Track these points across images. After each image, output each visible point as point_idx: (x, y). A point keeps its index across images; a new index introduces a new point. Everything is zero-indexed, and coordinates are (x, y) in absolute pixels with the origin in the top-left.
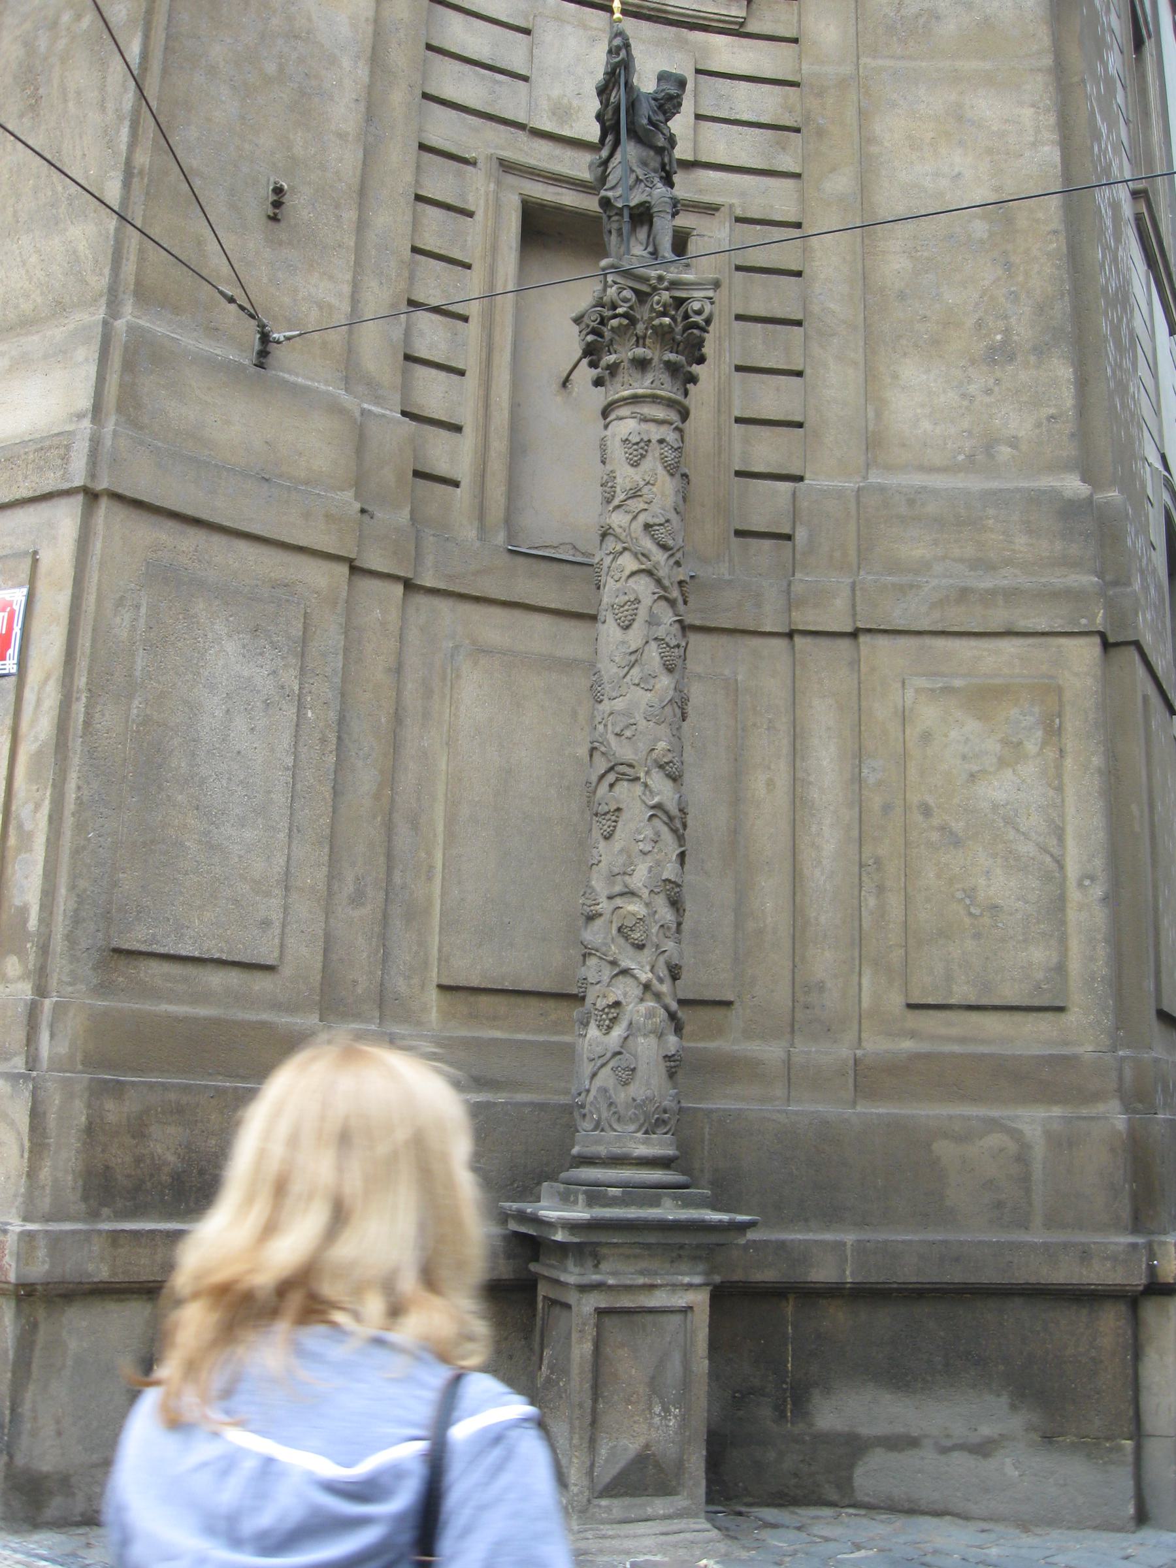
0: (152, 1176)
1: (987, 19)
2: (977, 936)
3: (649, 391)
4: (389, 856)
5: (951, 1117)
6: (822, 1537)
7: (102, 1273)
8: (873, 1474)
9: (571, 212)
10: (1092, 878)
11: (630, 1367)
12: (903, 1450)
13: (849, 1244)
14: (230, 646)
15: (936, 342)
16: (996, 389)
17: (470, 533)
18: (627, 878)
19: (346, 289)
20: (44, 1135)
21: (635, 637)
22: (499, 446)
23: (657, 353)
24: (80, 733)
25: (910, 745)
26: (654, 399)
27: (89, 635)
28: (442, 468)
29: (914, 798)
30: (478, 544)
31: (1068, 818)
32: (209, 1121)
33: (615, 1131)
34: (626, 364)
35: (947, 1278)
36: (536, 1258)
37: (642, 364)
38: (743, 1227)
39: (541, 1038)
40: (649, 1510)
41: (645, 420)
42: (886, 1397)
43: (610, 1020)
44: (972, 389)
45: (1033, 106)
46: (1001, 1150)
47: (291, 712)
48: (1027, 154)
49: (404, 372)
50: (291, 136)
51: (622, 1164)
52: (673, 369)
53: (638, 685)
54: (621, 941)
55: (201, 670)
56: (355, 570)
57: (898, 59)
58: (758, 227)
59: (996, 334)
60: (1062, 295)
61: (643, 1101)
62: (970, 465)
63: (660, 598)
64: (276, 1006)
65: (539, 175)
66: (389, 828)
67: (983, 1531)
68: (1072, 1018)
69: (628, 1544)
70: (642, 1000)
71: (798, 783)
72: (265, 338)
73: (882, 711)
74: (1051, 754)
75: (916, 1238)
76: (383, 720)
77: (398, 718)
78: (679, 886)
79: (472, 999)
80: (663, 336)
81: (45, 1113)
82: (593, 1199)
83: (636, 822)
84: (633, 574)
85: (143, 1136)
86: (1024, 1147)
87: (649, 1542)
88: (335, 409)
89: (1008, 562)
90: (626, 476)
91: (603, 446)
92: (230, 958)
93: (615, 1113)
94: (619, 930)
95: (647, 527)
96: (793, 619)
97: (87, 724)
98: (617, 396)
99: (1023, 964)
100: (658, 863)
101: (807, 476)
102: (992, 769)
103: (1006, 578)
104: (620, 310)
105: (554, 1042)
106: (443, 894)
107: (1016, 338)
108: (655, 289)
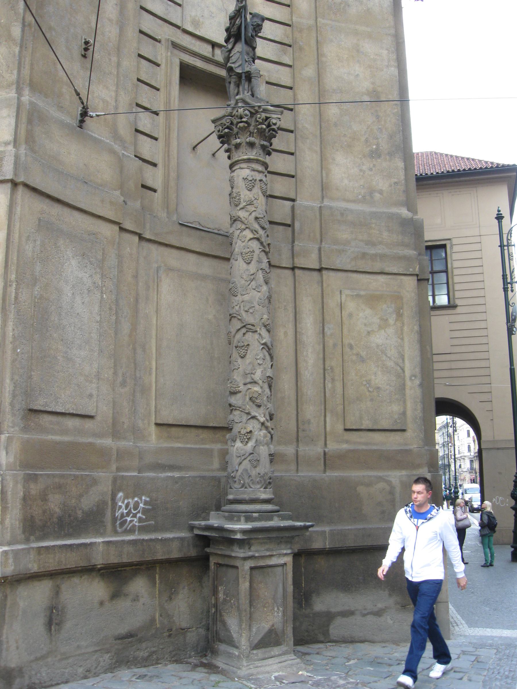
0: (50, 519)
1: (368, 9)
2: (372, 400)
3: (256, 158)
4: (135, 364)
5: (364, 476)
6: (331, 657)
7: (34, 568)
8: (336, 628)
9: (200, 70)
10: (415, 376)
11: (265, 592)
12: (348, 617)
13: (327, 531)
14: (74, 262)
15: (349, 146)
16: (374, 169)
17: (163, 215)
18: (252, 375)
19: (113, 94)
20: (6, 503)
21: (253, 268)
22: (173, 175)
23: (258, 141)
24: (13, 303)
25: (344, 319)
26: (257, 161)
27: (16, 254)
28: (150, 183)
29: (346, 341)
30: (167, 220)
31: (406, 351)
32: (72, 491)
33: (252, 488)
34: (244, 144)
35: (366, 544)
36: (208, 546)
37: (251, 145)
38: (306, 528)
39: (198, 446)
40: (272, 653)
41: (254, 170)
42: (341, 595)
43: (248, 439)
44: (364, 168)
45: (387, 50)
46: (383, 490)
47: (98, 295)
48: (385, 70)
49: (135, 136)
50: (90, 18)
51: (255, 503)
52: (263, 147)
53: (255, 289)
54: (251, 403)
55: (62, 274)
56: (122, 229)
57: (333, 21)
58: (275, 87)
59: (374, 145)
60: (399, 132)
61: (264, 474)
62: (364, 200)
63: (262, 251)
64: (95, 435)
65: (187, 51)
66: (134, 349)
67: (384, 647)
68: (409, 434)
69: (268, 669)
70: (261, 430)
71: (298, 334)
72: (84, 114)
73: (332, 303)
74: (399, 324)
75: (353, 527)
76: (132, 300)
77: (137, 300)
78: (272, 379)
79: (169, 429)
80: (261, 133)
81: (6, 492)
82: (248, 519)
83: (256, 351)
84: (251, 239)
85: (46, 500)
86: (392, 488)
87: (275, 667)
88: (112, 152)
89: (381, 243)
90: (245, 195)
91: (231, 181)
92: (77, 413)
93: (252, 480)
94: (250, 399)
95: (256, 218)
96: (295, 262)
97: (16, 298)
98: (240, 158)
99: (389, 412)
100: (265, 369)
101: (298, 199)
102: (376, 330)
103: (380, 250)
104: (244, 120)
105: (203, 449)
106: (156, 382)
107: (381, 148)
108: (257, 112)
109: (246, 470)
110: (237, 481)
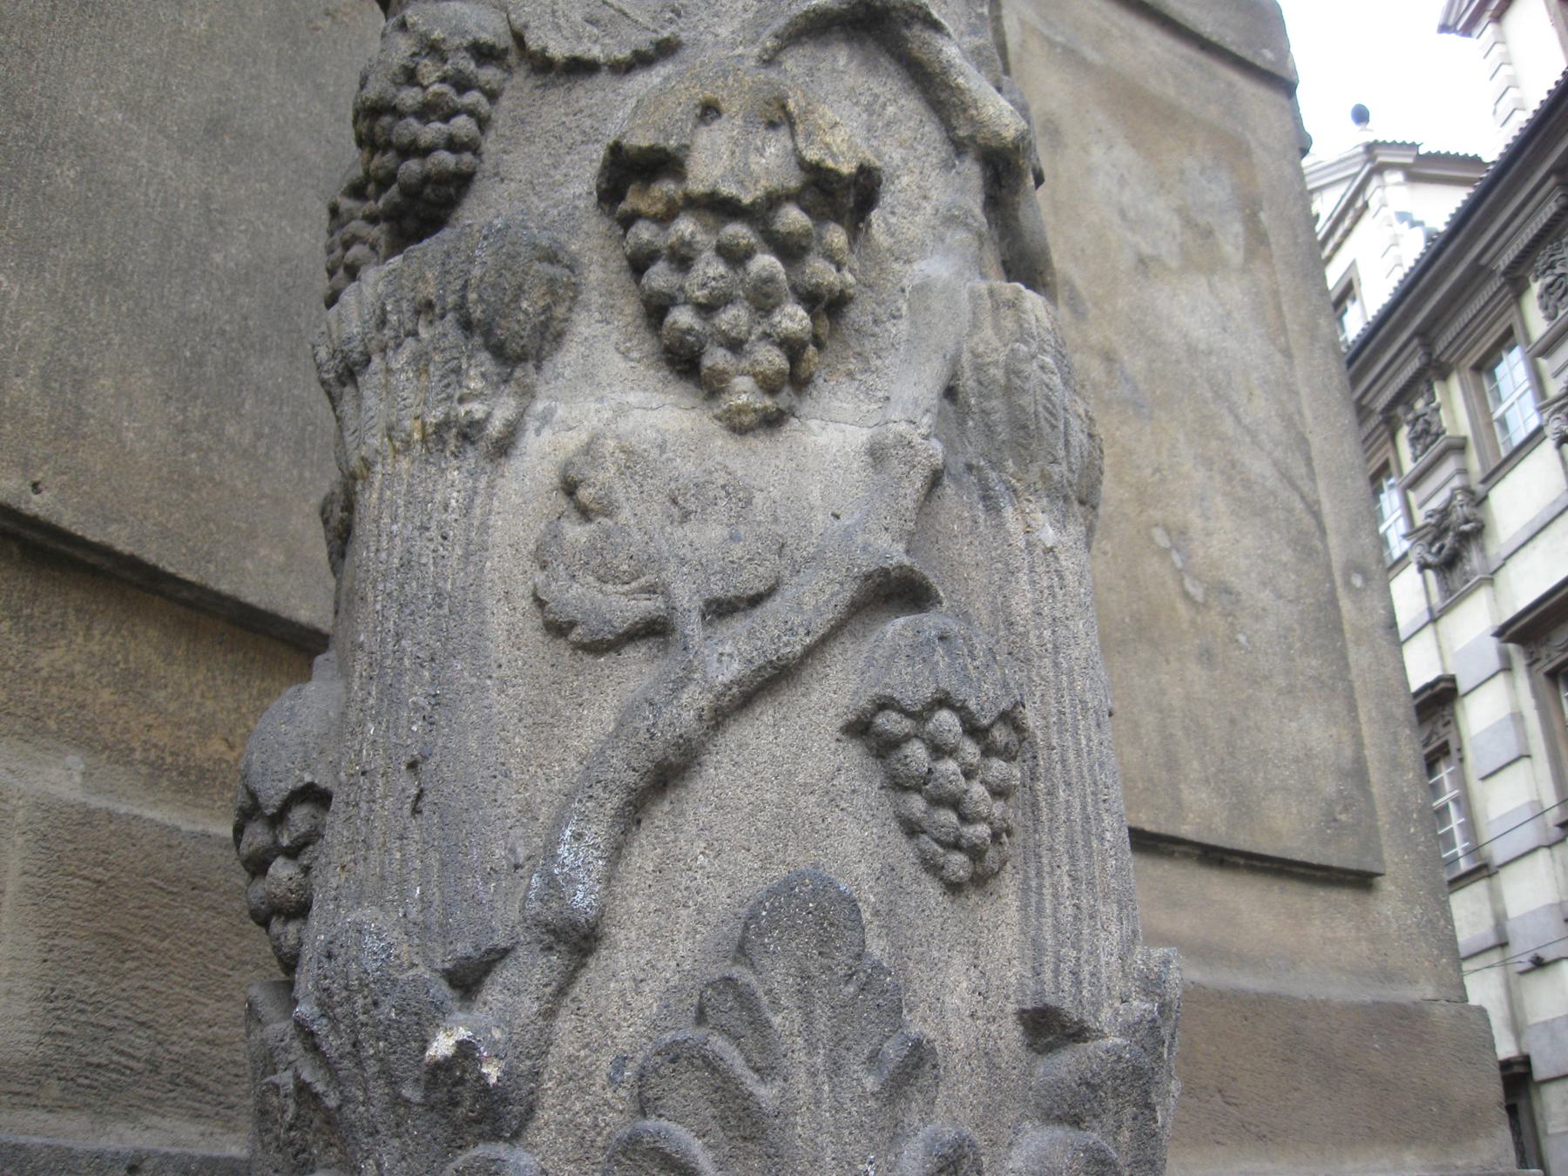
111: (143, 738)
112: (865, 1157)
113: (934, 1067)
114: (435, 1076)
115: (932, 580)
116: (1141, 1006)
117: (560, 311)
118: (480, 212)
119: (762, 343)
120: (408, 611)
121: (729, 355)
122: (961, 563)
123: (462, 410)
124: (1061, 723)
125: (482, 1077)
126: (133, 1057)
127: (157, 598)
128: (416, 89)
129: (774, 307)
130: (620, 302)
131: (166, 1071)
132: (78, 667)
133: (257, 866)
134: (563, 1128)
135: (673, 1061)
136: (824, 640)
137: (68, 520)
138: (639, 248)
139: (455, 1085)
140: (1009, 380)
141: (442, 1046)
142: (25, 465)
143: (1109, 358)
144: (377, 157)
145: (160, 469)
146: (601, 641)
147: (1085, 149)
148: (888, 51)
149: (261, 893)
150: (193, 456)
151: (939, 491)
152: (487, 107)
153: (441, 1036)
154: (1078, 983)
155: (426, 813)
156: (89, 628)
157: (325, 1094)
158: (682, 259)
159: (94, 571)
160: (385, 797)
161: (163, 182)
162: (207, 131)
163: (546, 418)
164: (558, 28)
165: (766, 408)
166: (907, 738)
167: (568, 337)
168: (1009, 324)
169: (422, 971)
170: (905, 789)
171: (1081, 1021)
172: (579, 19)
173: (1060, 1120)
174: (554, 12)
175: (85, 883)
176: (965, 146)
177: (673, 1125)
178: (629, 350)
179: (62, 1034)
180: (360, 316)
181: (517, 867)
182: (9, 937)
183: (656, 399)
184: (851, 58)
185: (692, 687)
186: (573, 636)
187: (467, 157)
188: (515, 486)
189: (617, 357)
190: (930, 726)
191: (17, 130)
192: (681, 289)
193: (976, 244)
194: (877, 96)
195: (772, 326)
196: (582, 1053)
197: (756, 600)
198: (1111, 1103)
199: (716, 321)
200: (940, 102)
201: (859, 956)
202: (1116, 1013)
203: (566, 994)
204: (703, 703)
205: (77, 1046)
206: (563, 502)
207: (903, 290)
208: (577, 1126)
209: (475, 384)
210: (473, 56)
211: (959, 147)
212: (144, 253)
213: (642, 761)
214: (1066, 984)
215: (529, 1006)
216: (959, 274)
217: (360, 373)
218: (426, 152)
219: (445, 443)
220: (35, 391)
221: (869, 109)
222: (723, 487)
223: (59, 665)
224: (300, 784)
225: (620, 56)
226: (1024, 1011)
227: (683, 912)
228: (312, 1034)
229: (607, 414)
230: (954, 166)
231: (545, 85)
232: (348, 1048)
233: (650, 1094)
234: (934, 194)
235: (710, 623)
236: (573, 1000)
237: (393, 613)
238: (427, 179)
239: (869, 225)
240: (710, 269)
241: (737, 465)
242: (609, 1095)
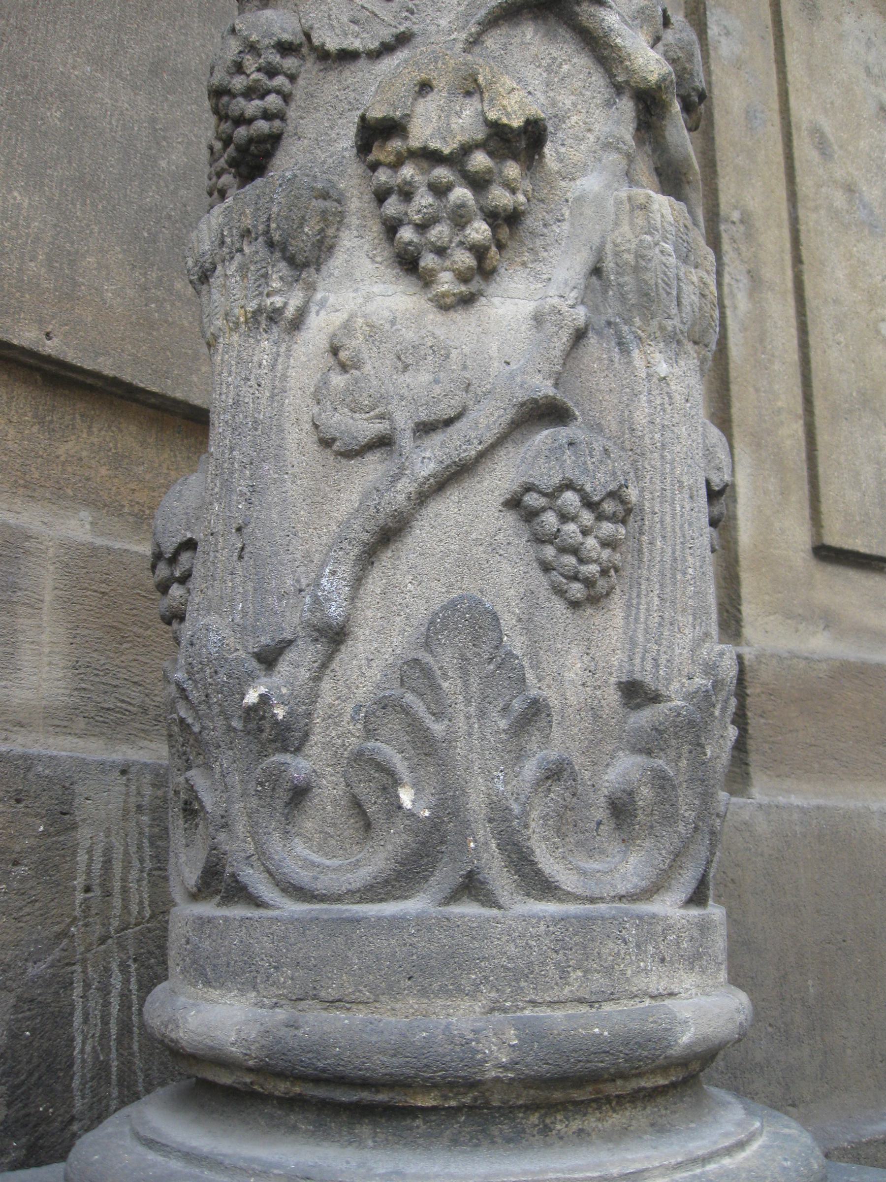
33: (542, 886)
43: (493, 217)
51: (605, 1102)
109: (467, 621)
110: (330, 790)
111: (129, 498)
112: (498, 768)
113: (548, 715)
114: (249, 714)
115: (570, 404)
116: (700, 681)
117: (331, 232)
118: (286, 163)
119: (459, 249)
120: (237, 433)
121: (436, 258)
122: (598, 390)
123: (269, 301)
124: (663, 496)
125: (274, 715)
126: (130, 704)
127: (134, 405)
128: (243, 77)
129: (467, 223)
130: (370, 223)
131: (152, 713)
132: (84, 454)
133: (163, 588)
134: (326, 746)
135: (383, 708)
136: (493, 447)
137: (72, 356)
138: (379, 186)
139: (260, 720)
140: (637, 262)
141: (252, 697)
142: (41, 321)
143: (850, 189)
144: (222, 123)
145: (130, 316)
146: (351, 450)
147: (838, 19)
148: (565, 23)
149: (166, 605)
150: (153, 306)
151: (584, 341)
152: (290, 87)
153: (251, 691)
154: (657, 666)
155: (246, 559)
156: (90, 427)
157: (193, 724)
158: (407, 194)
159: (91, 388)
160: (223, 549)
161: (122, 114)
162: (150, 71)
163: (322, 304)
164: (332, 27)
165: (462, 292)
166: (544, 510)
167: (338, 248)
168: (640, 222)
169: (242, 654)
170: (543, 542)
171: (657, 690)
172: (346, 20)
173: (640, 751)
174: (329, 16)
175: (95, 594)
176: (623, 88)
177: (384, 745)
178: (375, 255)
179: (84, 689)
180: (210, 238)
181: (301, 591)
182: (48, 629)
183: (391, 288)
184: (536, 32)
185: (404, 479)
186: (335, 447)
187: (277, 123)
188: (303, 350)
189: (368, 261)
190: (559, 502)
191: (18, 88)
192: (406, 214)
193: (625, 162)
194: (555, 59)
195: (465, 237)
196: (336, 702)
197: (449, 422)
198: (673, 742)
199: (428, 236)
200: (604, 57)
201: (497, 647)
202: (683, 685)
203: (328, 667)
204: (412, 489)
205: (94, 697)
206: (331, 361)
207: (567, 201)
208: (333, 745)
209: (276, 285)
210: (278, 51)
211: (619, 89)
212: (112, 166)
213: (371, 526)
214: (649, 666)
215: (304, 674)
216: (608, 186)
217: (212, 276)
218: (250, 121)
219: (259, 323)
220: (43, 270)
221: (549, 69)
222: (431, 347)
223: (72, 452)
224: (185, 539)
225: (372, 47)
226: (621, 683)
227: (398, 619)
228: (184, 690)
229: (361, 300)
230: (615, 103)
231: (325, 69)
232: (203, 698)
233: (371, 727)
234: (597, 127)
235: (420, 437)
236: (332, 671)
237: (228, 434)
238: (251, 140)
239: (542, 156)
240: (424, 200)
241: (441, 332)
242: (351, 727)
